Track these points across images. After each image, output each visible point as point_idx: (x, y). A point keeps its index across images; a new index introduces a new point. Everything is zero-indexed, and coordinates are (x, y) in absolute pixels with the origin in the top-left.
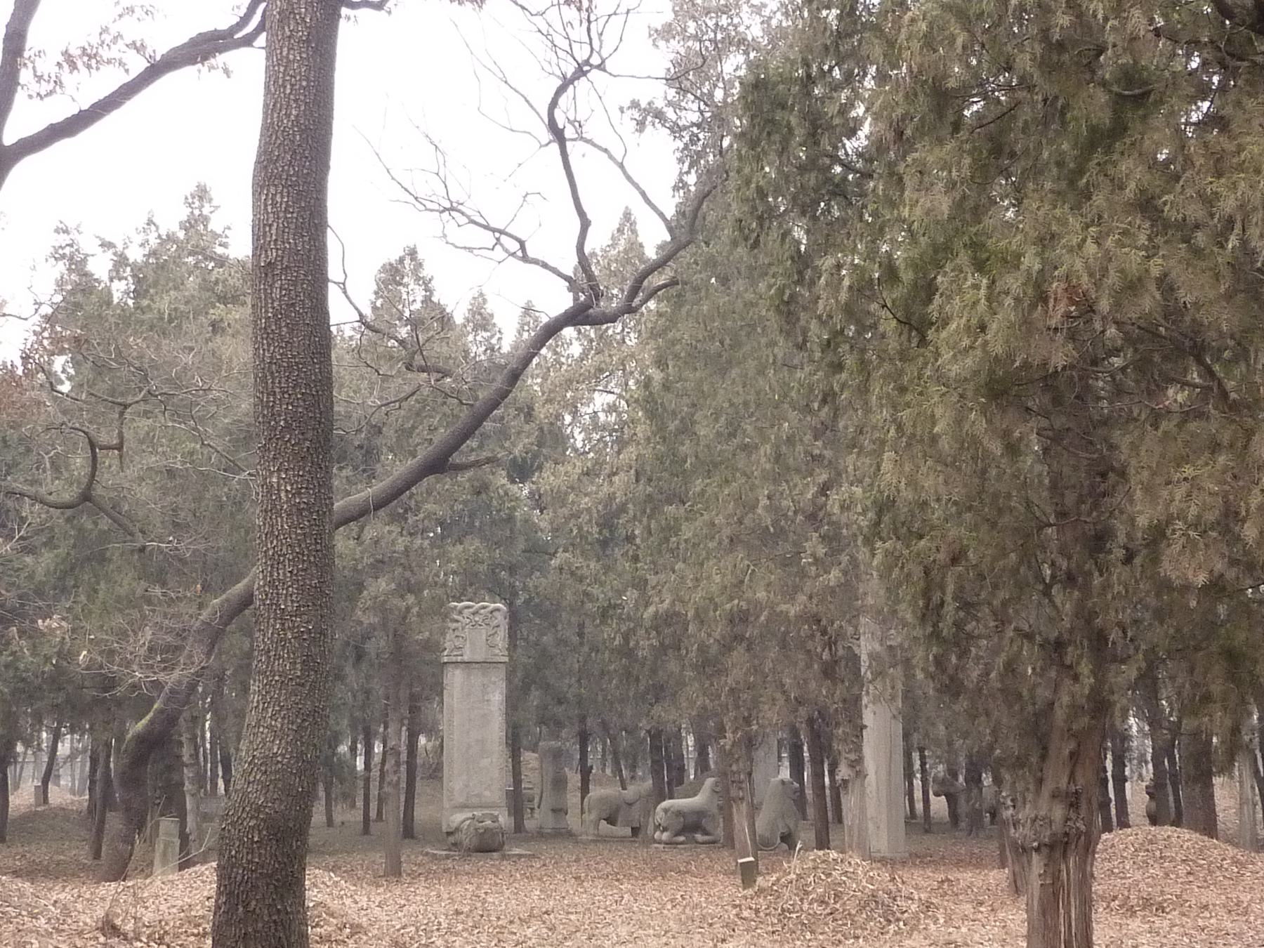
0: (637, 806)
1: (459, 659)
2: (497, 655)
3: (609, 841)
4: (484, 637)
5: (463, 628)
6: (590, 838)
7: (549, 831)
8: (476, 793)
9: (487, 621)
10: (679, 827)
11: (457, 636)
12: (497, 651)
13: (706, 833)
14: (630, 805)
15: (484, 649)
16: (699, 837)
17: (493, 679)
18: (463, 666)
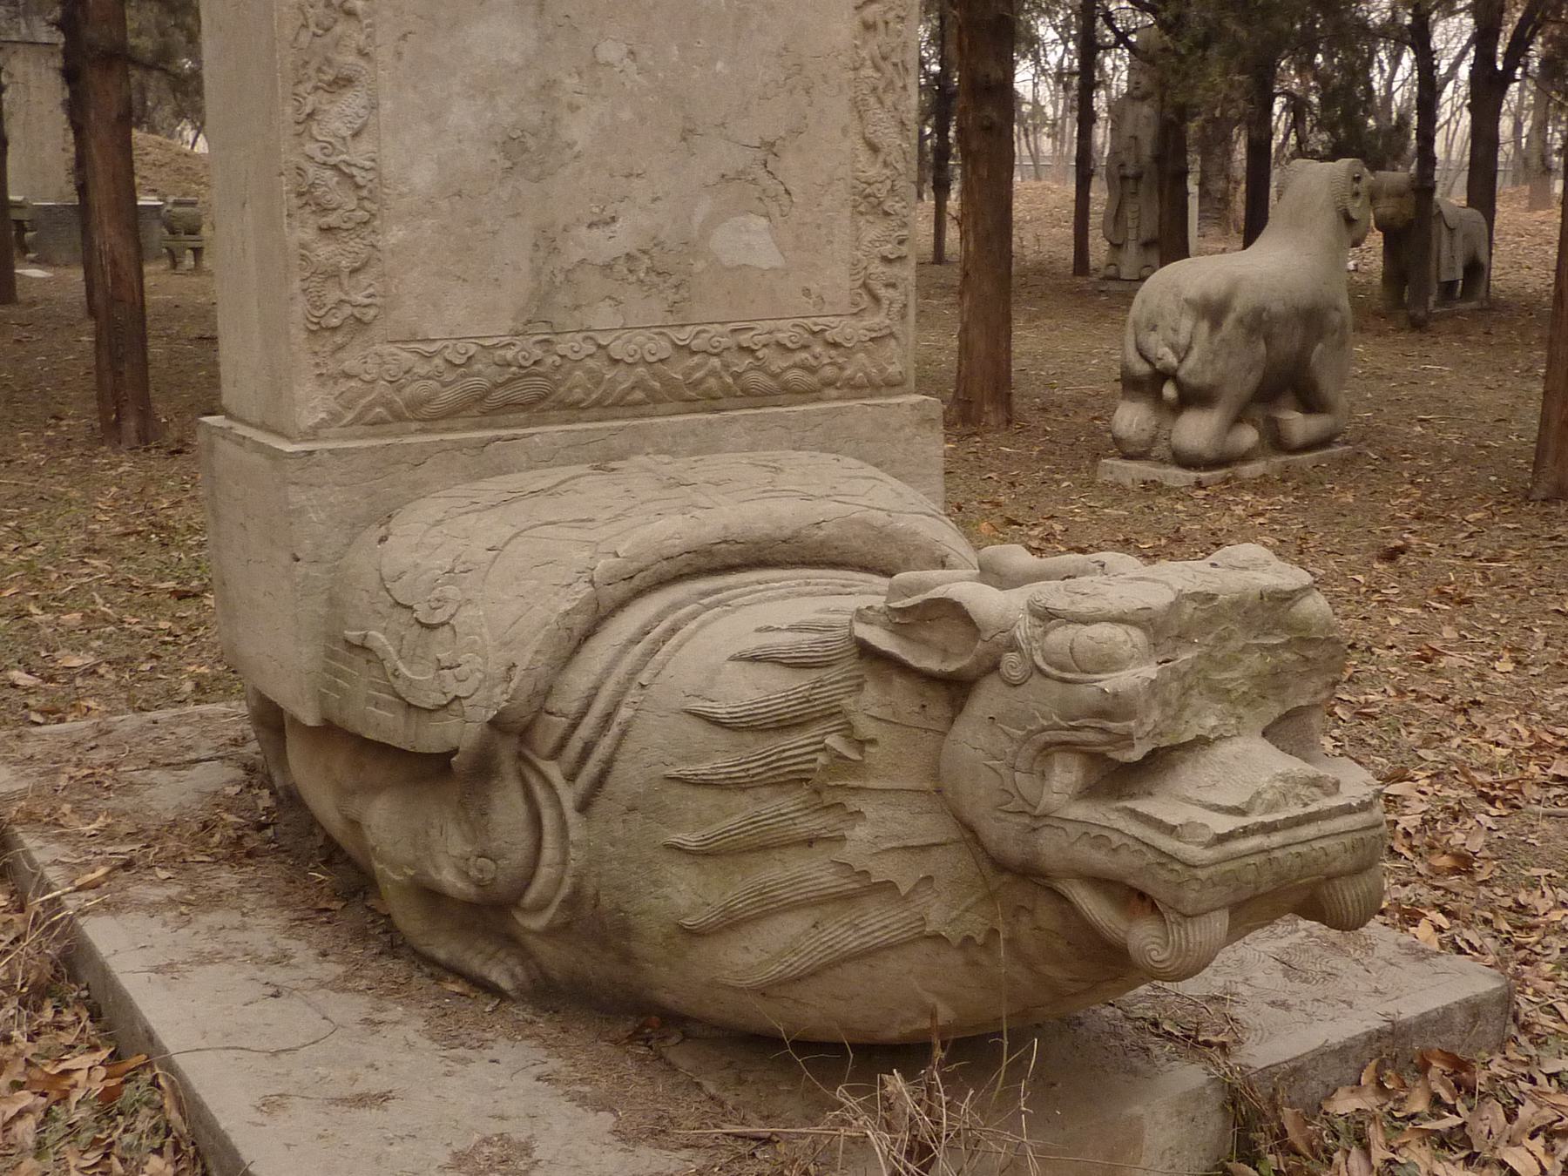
10: (1253, 380)
13: (1311, 403)
16: (1299, 425)
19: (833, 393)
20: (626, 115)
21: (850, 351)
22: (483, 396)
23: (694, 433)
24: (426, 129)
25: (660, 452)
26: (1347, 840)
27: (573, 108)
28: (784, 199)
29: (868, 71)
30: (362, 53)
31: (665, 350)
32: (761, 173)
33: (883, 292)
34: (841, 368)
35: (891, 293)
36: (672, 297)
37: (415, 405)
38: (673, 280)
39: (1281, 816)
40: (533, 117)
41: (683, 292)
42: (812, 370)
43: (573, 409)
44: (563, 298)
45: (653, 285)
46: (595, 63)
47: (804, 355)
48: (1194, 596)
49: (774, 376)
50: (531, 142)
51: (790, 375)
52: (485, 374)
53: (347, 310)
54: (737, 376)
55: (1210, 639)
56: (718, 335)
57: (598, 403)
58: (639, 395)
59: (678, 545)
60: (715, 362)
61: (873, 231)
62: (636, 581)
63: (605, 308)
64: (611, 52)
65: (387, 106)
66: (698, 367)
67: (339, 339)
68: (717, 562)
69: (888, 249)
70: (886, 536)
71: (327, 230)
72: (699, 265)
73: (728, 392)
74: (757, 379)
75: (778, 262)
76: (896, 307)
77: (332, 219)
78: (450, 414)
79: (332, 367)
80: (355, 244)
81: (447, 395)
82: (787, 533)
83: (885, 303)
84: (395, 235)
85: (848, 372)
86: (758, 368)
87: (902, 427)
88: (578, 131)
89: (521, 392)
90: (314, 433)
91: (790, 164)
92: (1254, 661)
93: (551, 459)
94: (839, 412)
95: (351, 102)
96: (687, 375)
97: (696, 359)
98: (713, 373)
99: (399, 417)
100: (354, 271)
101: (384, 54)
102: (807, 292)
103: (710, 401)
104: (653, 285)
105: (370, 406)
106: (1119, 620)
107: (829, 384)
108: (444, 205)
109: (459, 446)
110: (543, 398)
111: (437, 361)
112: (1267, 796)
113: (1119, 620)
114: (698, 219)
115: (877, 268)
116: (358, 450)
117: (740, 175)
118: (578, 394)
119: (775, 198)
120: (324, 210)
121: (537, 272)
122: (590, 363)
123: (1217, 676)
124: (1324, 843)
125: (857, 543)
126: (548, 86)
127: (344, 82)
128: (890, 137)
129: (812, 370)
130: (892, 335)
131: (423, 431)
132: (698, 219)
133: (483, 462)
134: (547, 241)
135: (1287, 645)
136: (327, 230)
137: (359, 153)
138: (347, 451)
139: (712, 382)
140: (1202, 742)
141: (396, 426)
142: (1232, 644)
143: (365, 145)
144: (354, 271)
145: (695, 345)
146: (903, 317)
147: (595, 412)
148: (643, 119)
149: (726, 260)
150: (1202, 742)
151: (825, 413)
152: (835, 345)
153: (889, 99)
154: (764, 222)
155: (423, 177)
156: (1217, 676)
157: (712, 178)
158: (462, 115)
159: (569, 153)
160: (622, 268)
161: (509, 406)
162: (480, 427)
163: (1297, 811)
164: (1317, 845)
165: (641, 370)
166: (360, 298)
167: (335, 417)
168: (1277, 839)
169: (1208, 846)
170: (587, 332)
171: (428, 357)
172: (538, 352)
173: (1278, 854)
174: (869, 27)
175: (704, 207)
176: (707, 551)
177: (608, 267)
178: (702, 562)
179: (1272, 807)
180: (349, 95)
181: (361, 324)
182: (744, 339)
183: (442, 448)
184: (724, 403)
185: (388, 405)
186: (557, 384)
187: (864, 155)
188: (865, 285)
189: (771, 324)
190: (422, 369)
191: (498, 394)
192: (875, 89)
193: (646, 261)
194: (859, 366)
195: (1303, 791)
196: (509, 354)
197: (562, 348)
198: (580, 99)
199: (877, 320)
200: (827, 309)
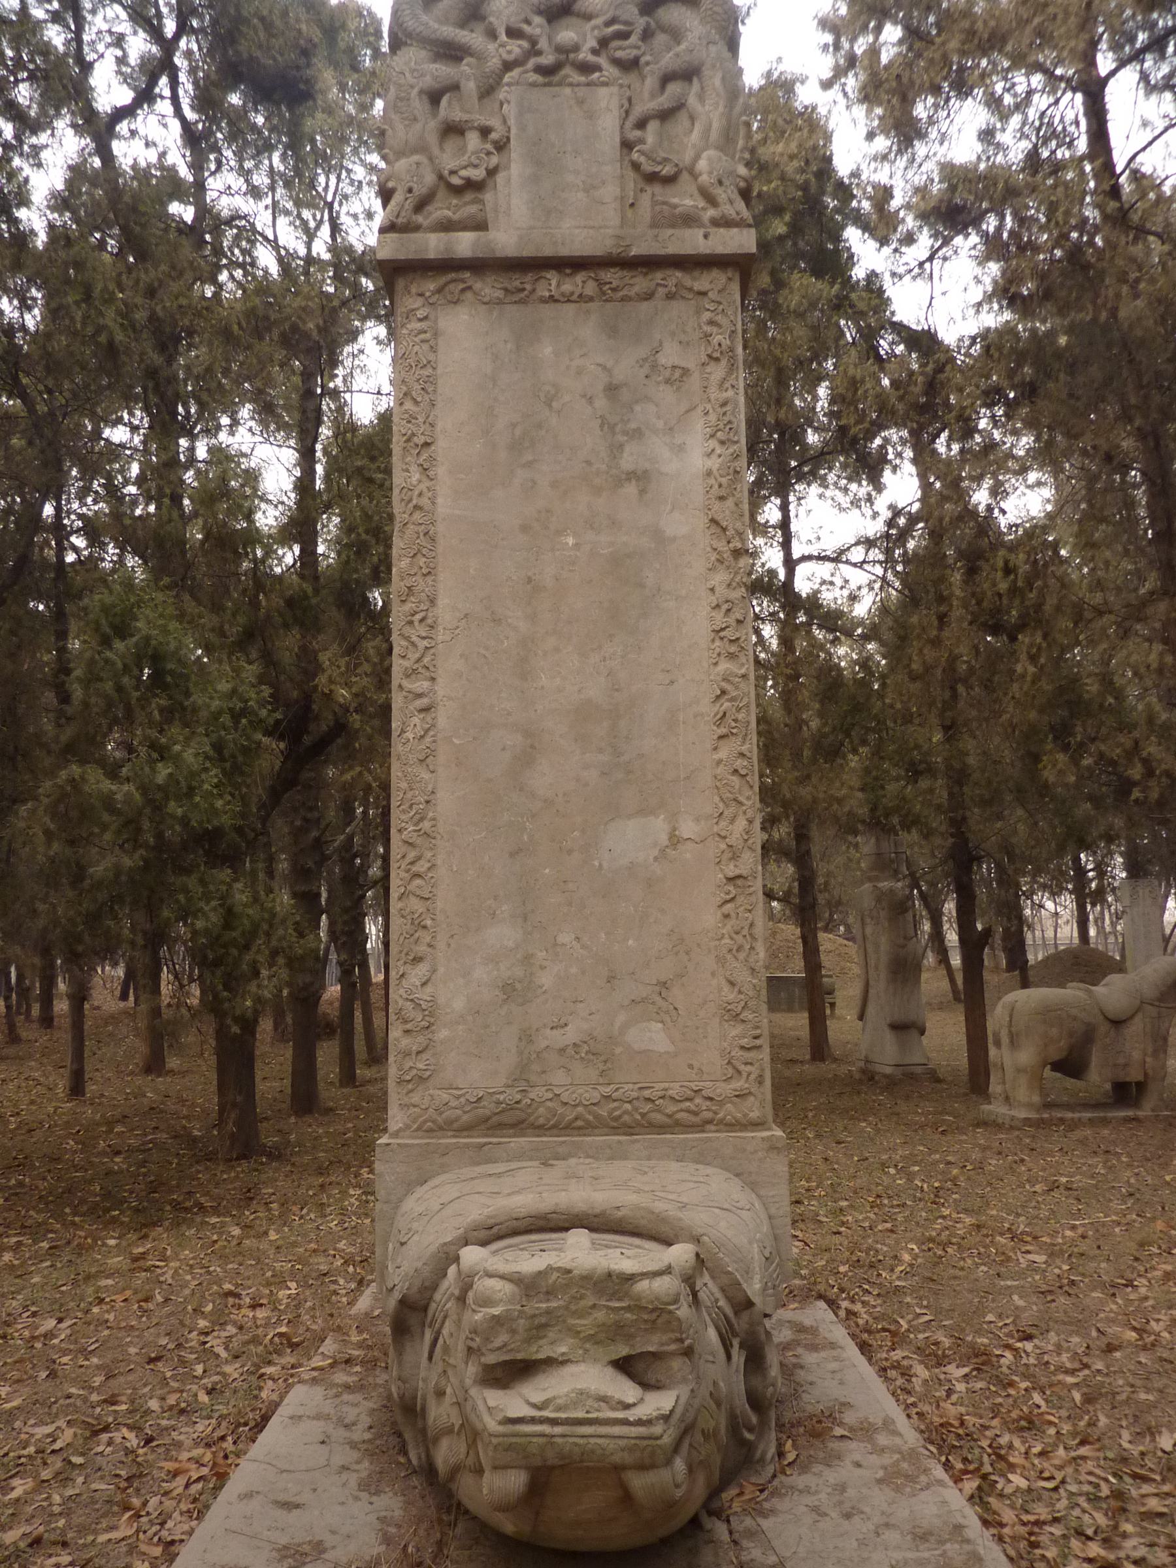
0: (1136, 1027)
1: (465, 244)
2: (689, 220)
3: (1073, 1126)
4: (609, 125)
5: (487, 92)
6: (1022, 1114)
7: (888, 1070)
8: (571, 1035)
9: (625, 52)
11: (452, 130)
12: (685, 199)
14: (1117, 1023)
15: (610, 192)
17: (671, 355)
18: (488, 287)
19: (713, 1128)
20: (574, 970)
21: (721, 1103)
22: (488, 1119)
23: (610, 1147)
24: (461, 981)
25: (588, 1157)
26: (622, 1443)
27: (542, 968)
28: (674, 1012)
29: (727, 941)
30: (430, 946)
31: (596, 1097)
32: (658, 999)
33: (742, 1068)
34: (716, 1113)
35: (749, 1068)
36: (601, 1067)
37: (450, 1122)
38: (603, 1058)
39: (563, 1415)
40: (519, 972)
41: (609, 1065)
42: (696, 1114)
43: (540, 1129)
44: (536, 1067)
45: (589, 1061)
46: (555, 945)
47: (688, 1104)
48: (559, 1269)
49: (670, 1116)
50: (518, 986)
51: (679, 1116)
52: (487, 1108)
53: (414, 1072)
54: (643, 1115)
55: (566, 1297)
56: (630, 1091)
57: (554, 1127)
58: (579, 1123)
59: (523, 1212)
60: (628, 1106)
61: (735, 1030)
62: (495, 1230)
63: (561, 1072)
64: (565, 938)
65: (441, 970)
66: (615, 1109)
67: (410, 1086)
68: (552, 1225)
69: (745, 1042)
70: (663, 1219)
71: (407, 1032)
72: (618, 1050)
73: (639, 1124)
74: (658, 1117)
75: (671, 1049)
76: (753, 1077)
77: (409, 1026)
78: (467, 1129)
79: (406, 1100)
80: (420, 1039)
81: (465, 1118)
82: (597, 1211)
83: (745, 1075)
84: (443, 1034)
85: (720, 1116)
86: (659, 1111)
87: (756, 1152)
88: (546, 980)
89: (506, 1118)
90: (396, 1135)
91: (676, 994)
92: (600, 1315)
93: (520, 1156)
94: (709, 1139)
95: (422, 970)
96: (610, 1113)
97: (616, 1104)
98: (626, 1112)
99: (441, 1128)
100: (419, 1053)
101: (441, 945)
102: (691, 1066)
103: (629, 1129)
104: (589, 1061)
105: (425, 1122)
106: (502, 1277)
107: (710, 1122)
108: (470, 1018)
109: (467, 1146)
110: (523, 1122)
111: (462, 1100)
112: (559, 1401)
113: (502, 1277)
114: (617, 1025)
115: (737, 1053)
116: (412, 1146)
117: (643, 1000)
118: (541, 1121)
119: (667, 1012)
120: (406, 1022)
121: (520, 1053)
122: (549, 1104)
123: (571, 1321)
124: (599, 1441)
125: (643, 1222)
126: (528, 959)
127: (417, 960)
128: (743, 977)
129: (696, 1114)
130: (750, 1093)
131: (455, 1136)
132: (617, 1025)
133: (481, 1156)
134: (527, 1037)
135: (628, 1309)
136: (407, 1032)
137: (424, 995)
138: (406, 1145)
139: (626, 1118)
140: (550, 1362)
141: (439, 1134)
142: (583, 1303)
143: (429, 989)
144: (419, 1053)
145: (615, 1095)
146: (760, 1083)
147: (555, 1131)
148: (583, 973)
149: (636, 1047)
150: (550, 1362)
151: (701, 1139)
152: (711, 1099)
153: (741, 956)
154: (660, 1025)
155: (459, 1004)
156: (571, 1321)
157: (626, 1002)
158: (481, 973)
159: (540, 991)
160: (570, 1051)
161: (501, 1126)
162: (487, 1136)
163: (580, 1414)
164: (592, 1441)
165: (580, 1109)
166: (421, 1066)
167: (408, 1127)
168: (558, 1430)
169: (500, 1423)
170: (549, 1086)
171: (458, 1097)
172: (518, 1097)
173: (559, 1440)
174: (727, 916)
175: (621, 1018)
176: (544, 1217)
177: (562, 1051)
178: (542, 1223)
179: (559, 1409)
180: (421, 965)
181: (422, 1080)
182: (647, 1093)
183: (457, 1146)
184: (637, 1130)
185: (434, 1122)
186: (529, 1115)
187: (726, 988)
188: (729, 1063)
189: (663, 1085)
190: (454, 1103)
191: (495, 1119)
192: (730, 951)
193: (586, 1047)
194: (730, 1111)
195: (590, 1402)
196: (502, 1097)
197: (532, 1095)
198: (545, 963)
199: (739, 1084)
200: (705, 1077)
